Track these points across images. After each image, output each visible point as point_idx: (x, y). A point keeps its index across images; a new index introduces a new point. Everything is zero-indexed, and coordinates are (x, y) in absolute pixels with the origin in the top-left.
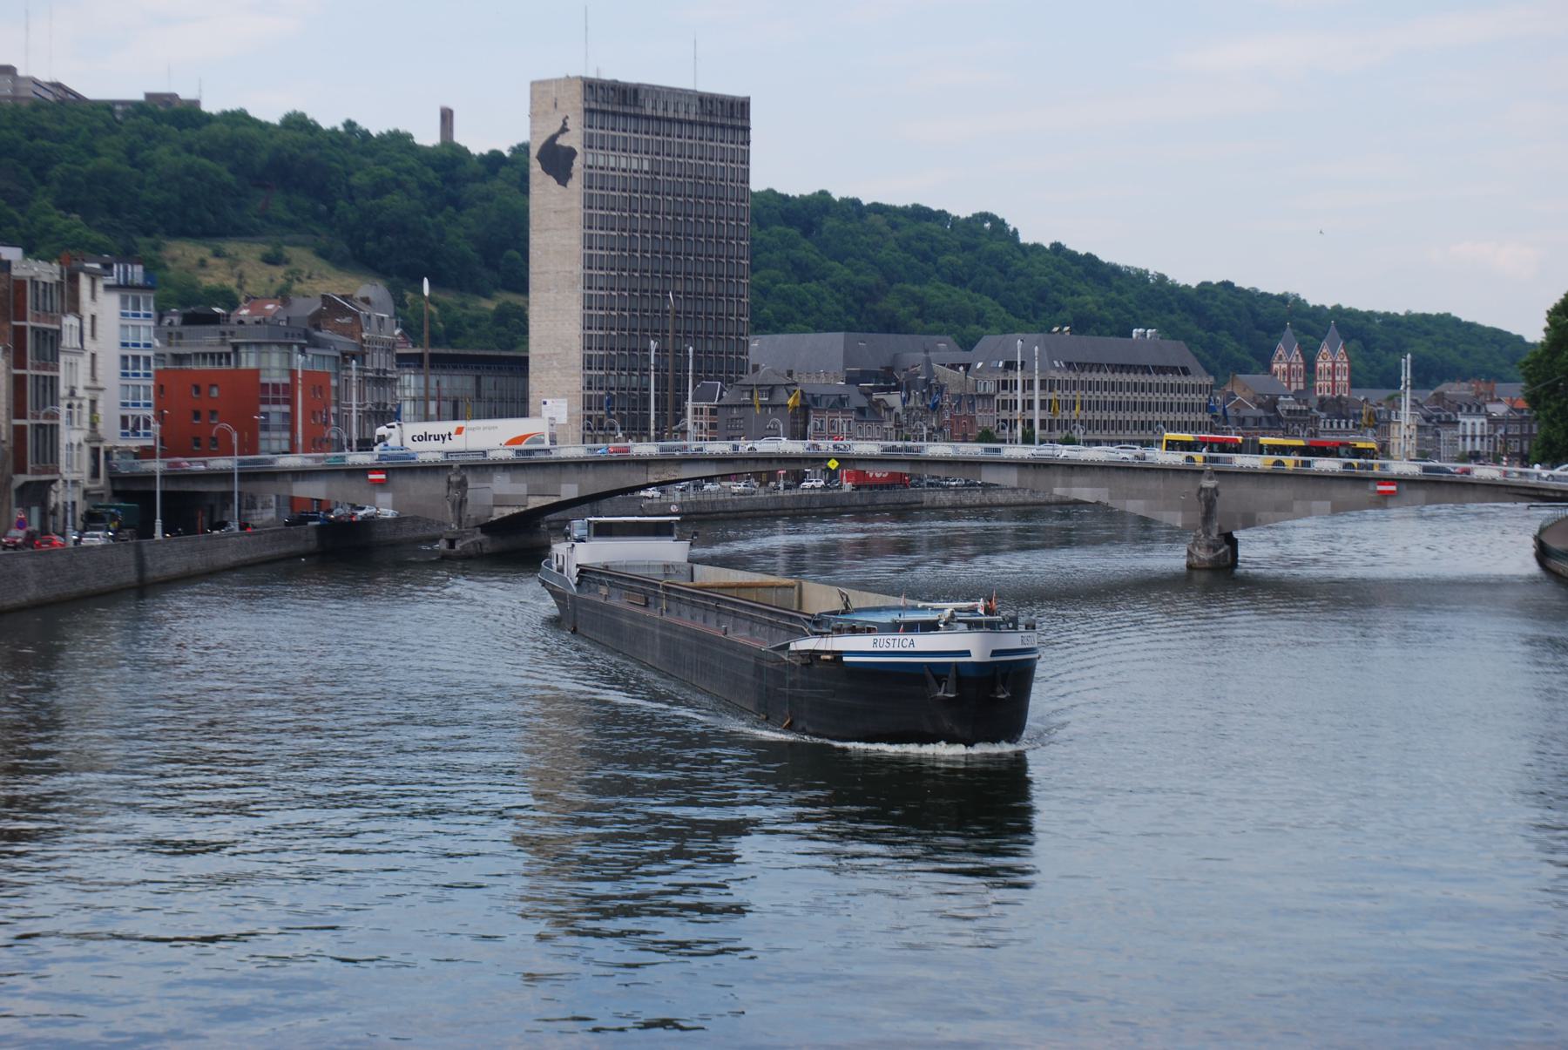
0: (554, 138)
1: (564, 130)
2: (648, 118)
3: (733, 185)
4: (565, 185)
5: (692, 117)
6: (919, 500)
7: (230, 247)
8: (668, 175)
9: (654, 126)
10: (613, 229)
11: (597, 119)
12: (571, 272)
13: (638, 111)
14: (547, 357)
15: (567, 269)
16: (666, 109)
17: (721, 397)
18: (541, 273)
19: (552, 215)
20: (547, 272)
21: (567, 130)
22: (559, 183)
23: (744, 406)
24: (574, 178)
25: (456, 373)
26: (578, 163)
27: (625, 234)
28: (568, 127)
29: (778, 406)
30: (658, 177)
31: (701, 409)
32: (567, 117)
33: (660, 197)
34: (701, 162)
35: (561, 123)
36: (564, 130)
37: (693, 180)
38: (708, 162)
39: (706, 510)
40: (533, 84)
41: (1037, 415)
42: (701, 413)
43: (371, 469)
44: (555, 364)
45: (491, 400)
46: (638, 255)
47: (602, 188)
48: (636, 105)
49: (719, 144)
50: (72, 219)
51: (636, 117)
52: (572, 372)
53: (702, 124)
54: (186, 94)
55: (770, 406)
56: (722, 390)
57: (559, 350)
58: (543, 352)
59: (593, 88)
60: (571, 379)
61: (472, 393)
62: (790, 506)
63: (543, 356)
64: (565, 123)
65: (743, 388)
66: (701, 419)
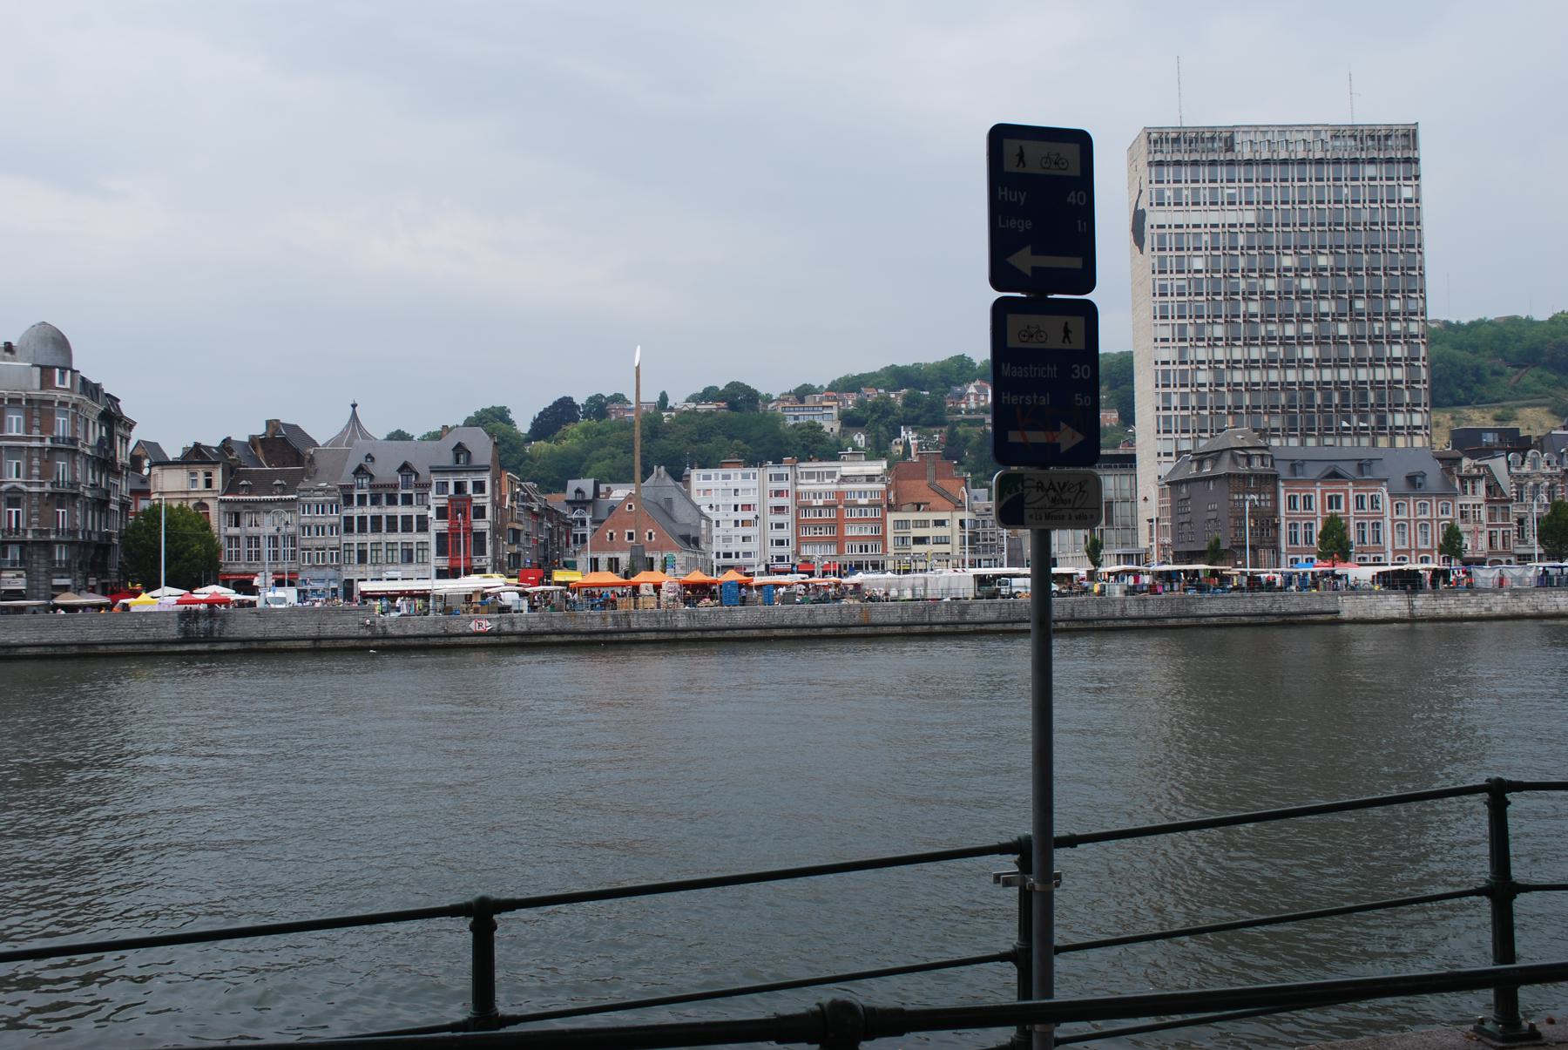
2: (1249, 163)
6: (1331, 608)
11: (1168, 173)
13: (1229, 156)
39: (596, 628)
51: (1231, 163)
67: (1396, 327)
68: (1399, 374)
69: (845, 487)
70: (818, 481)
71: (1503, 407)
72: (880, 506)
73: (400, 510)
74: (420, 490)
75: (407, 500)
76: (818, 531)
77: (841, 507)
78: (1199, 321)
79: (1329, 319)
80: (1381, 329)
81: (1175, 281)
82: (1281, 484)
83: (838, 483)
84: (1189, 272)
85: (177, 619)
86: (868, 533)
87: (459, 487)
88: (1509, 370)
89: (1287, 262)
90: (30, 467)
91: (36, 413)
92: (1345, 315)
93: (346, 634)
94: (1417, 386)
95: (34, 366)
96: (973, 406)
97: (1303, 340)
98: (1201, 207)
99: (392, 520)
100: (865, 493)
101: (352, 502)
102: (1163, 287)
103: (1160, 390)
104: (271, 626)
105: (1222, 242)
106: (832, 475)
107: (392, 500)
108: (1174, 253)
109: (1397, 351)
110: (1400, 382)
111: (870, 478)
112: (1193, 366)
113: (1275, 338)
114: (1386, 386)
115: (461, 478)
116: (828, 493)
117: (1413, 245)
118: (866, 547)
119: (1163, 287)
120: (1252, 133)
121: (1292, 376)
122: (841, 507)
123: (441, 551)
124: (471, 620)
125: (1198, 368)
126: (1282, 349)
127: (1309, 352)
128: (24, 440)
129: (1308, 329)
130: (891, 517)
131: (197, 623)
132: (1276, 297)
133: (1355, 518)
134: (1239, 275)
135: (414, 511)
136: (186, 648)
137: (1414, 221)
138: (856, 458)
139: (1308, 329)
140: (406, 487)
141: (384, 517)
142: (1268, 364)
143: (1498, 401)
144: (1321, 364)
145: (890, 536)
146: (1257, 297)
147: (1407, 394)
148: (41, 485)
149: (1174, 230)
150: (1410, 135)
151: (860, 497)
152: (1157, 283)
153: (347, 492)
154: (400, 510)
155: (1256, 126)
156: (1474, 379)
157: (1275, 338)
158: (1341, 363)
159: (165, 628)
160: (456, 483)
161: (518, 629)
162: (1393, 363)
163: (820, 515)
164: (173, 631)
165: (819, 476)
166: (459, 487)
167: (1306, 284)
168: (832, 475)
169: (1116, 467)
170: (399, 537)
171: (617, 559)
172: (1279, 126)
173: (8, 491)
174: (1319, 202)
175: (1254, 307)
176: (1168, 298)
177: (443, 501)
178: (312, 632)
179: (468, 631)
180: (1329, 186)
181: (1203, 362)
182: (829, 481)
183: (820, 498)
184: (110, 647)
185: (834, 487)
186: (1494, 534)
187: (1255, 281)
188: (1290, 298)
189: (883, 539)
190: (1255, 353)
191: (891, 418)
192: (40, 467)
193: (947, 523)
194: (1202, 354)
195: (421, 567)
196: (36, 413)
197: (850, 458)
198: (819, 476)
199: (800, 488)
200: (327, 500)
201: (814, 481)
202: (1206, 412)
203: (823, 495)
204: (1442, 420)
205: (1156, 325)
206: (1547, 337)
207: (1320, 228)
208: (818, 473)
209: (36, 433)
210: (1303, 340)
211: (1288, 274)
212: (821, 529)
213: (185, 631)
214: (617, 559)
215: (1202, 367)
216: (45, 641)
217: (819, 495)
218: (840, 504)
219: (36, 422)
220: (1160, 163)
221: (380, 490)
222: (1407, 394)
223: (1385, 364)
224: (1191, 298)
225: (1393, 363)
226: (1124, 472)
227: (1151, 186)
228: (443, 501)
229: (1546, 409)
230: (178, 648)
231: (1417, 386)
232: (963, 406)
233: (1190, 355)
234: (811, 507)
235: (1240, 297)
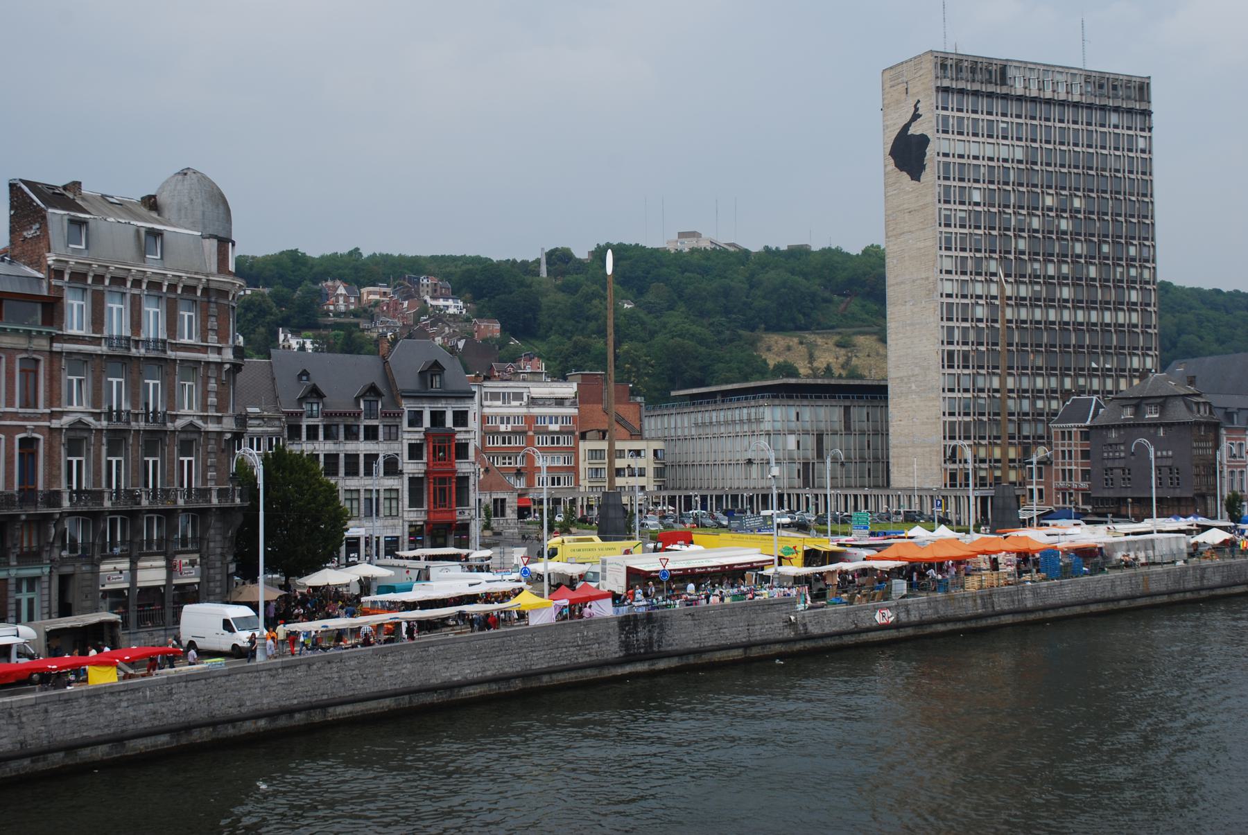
0: (906, 127)
1: (916, 116)
2: (1020, 99)
3: (1132, 176)
5: (1076, 98)
7: (810, 337)
8: (1048, 164)
9: (1026, 108)
10: (978, 227)
11: (953, 100)
12: (927, 279)
13: (1005, 90)
14: (906, 380)
17: (1096, 414)
19: (907, 216)
20: (902, 283)
23: (1125, 426)
24: (928, 169)
25: (820, 403)
26: (931, 151)
27: (994, 233)
28: (920, 112)
29: (1173, 424)
31: (1070, 433)
32: (919, 101)
33: (1039, 190)
34: (1091, 150)
35: (913, 109)
36: (916, 116)
37: (1080, 171)
38: (1099, 151)
39: (971, 612)
41: (1061, 449)
42: (1070, 439)
44: (914, 387)
45: (862, 433)
46: (1012, 257)
47: (962, 180)
51: (1005, 97)
52: (933, 395)
53: (1090, 107)
54: (827, 246)
55: (1162, 424)
56: (1098, 406)
57: (917, 371)
58: (901, 374)
59: (944, 63)
60: (930, 404)
61: (839, 426)
62: (1163, 588)
63: (901, 379)
64: (916, 109)
65: (1124, 402)
67: (1133, 272)
68: (1135, 318)
69: (536, 411)
70: (504, 403)
71: (840, 333)
72: (572, 433)
73: (362, 447)
74: (389, 421)
75: (371, 434)
76: (507, 461)
77: (531, 433)
78: (978, 255)
79: (1083, 261)
80: (1122, 273)
81: (959, 212)
82: (1223, 432)
83: (528, 406)
84: (970, 204)
85: (617, 629)
86: (561, 464)
87: (437, 418)
88: (836, 298)
89: (1049, 201)
90: (205, 394)
91: (213, 309)
92: (1094, 258)
93: (772, 636)
94: (1149, 331)
95: (203, 237)
96: (342, 308)
97: (1062, 280)
98: (980, 139)
99: (352, 459)
100: (557, 418)
101: (300, 437)
102: (947, 217)
103: (946, 324)
104: (705, 631)
105: (997, 174)
106: (518, 396)
107: (351, 434)
108: (957, 184)
109: (1134, 296)
110: (1136, 326)
111: (560, 402)
112: (973, 301)
113: (1039, 277)
114: (1126, 329)
115: (439, 406)
116: (517, 417)
117: (1146, 191)
118: (559, 479)
119: (947, 217)
120: (1022, 69)
121: (1052, 315)
122: (531, 433)
123: (415, 501)
124: (875, 609)
125: (977, 303)
126: (1044, 288)
127: (1066, 293)
128: (199, 351)
129: (1065, 269)
130: (584, 446)
131: (637, 632)
132: (1040, 236)
133: (1229, 466)
134: (1010, 211)
135: (381, 448)
136: (628, 669)
137: (1147, 171)
138: (536, 378)
139: (1065, 269)
140: (369, 416)
141: (342, 456)
142: (1034, 302)
143: (832, 327)
144: (1077, 304)
145: (584, 465)
146: (1025, 235)
147: (1073, 336)
148: (219, 420)
149: (986, 162)
150: (1142, 88)
151: (551, 423)
152: (943, 212)
153: (293, 421)
154: (362, 447)
155: (1026, 63)
156: (812, 305)
157: (1039, 277)
158: (1091, 305)
159: (607, 643)
160: (431, 412)
161: (913, 618)
162: (1132, 307)
163: (510, 443)
164: (613, 649)
165: (504, 398)
166: (437, 418)
167: (1064, 225)
168: (518, 396)
169: (825, 397)
170: (362, 482)
171: (503, 501)
172: (1044, 65)
173: (184, 430)
174: (1062, 143)
175: (1022, 245)
176: (952, 230)
177: (417, 436)
178: (742, 638)
179: (874, 624)
180: (1027, 124)
181: (980, 297)
182: (517, 403)
183: (508, 423)
184: (554, 676)
185: (524, 410)
186: (334, 428)
187: (1022, 218)
188: (1051, 238)
189: (574, 470)
190: (1023, 291)
191: (269, 318)
192: (217, 394)
193: (643, 454)
194: (979, 289)
195: (390, 522)
196: (213, 309)
197: (530, 377)
198: (504, 398)
199: (486, 410)
200: (266, 432)
201: (499, 403)
202: (983, 348)
203: (560, 420)
204: (791, 344)
205: (941, 256)
206: (869, 269)
207: (1076, 171)
208: (504, 394)
209: (213, 340)
210: (1062, 280)
211: (1051, 214)
212: (510, 458)
213: (626, 645)
214: (503, 501)
215: (980, 302)
216: (489, 673)
217: (506, 419)
218: (530, 429)
219: (213, 323)
220: (946, 90)
221: (337, 420)
222: (1073, 336)
223: (1125, 308)
224: (971, 231)
225: (1132, 307)
226: (834, 404)
227: (938, 112)
228: (417, 436)
229: (875, 337)
230: (619, 671)
231: (1149, 331)
232: (332, 308)
233: (969, 290)
234: (499, 433)
235: (1011, 233)
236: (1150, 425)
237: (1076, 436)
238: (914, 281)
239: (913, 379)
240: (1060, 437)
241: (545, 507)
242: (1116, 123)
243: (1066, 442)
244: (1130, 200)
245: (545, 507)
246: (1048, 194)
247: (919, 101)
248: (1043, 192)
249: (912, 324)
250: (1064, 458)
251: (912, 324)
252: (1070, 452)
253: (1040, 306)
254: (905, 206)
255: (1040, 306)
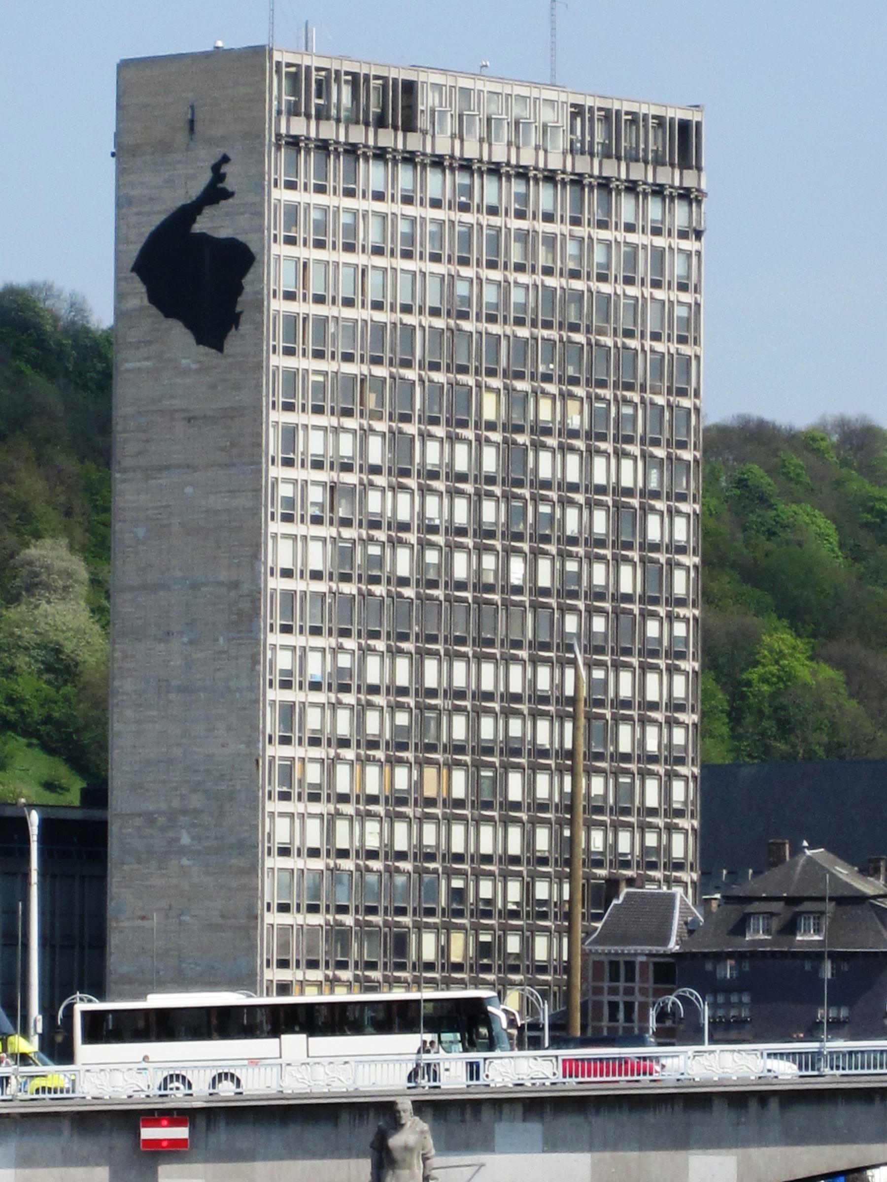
4: (219, 347)
13: (414, 142)
15: (223, 575)
16: (486, 139)
18: (144, 587)
19: (180, 428)
20: (160, 586)
21: (227, 195)
22: (200, 341)
28: (229, 184)
30: (467, 326)
31: (630, 965)
32: (225, 159)
35: (206, 177)
40: (124, 66)
42: (630, 978)
43: (151, 1112)
44: (185, 839)
48: (409, 126)
49: (621, 236)
50: (779, 646)
57: (197, 801)
60: (234, 883)
63: (150, 818)
64: (218, 175)
66: (614, 991)
236: (806, 955)
237: (644, 973)
238: (195, 586)
239: (184, 820)
240: (607, 975)
241: (652, 1024)
242: (631, 220)
243: (622, 984)
244: (653, 404)
245: (652, 1024)
246: (489, 389)
247: (225, 159)
248: (478, 385)
249: (184, 690)
250: (613, 1017)
251: (184, 690)
252: (629, 1006)
253: (436, 653)
254: (178, 403)
255: (436, 653)
